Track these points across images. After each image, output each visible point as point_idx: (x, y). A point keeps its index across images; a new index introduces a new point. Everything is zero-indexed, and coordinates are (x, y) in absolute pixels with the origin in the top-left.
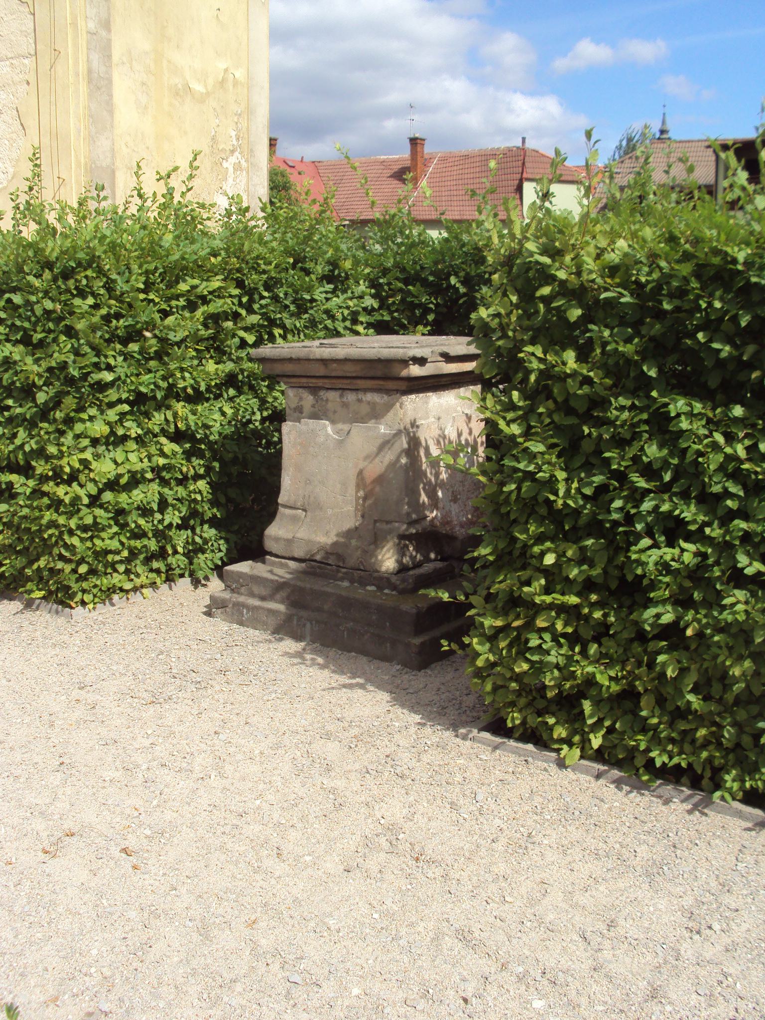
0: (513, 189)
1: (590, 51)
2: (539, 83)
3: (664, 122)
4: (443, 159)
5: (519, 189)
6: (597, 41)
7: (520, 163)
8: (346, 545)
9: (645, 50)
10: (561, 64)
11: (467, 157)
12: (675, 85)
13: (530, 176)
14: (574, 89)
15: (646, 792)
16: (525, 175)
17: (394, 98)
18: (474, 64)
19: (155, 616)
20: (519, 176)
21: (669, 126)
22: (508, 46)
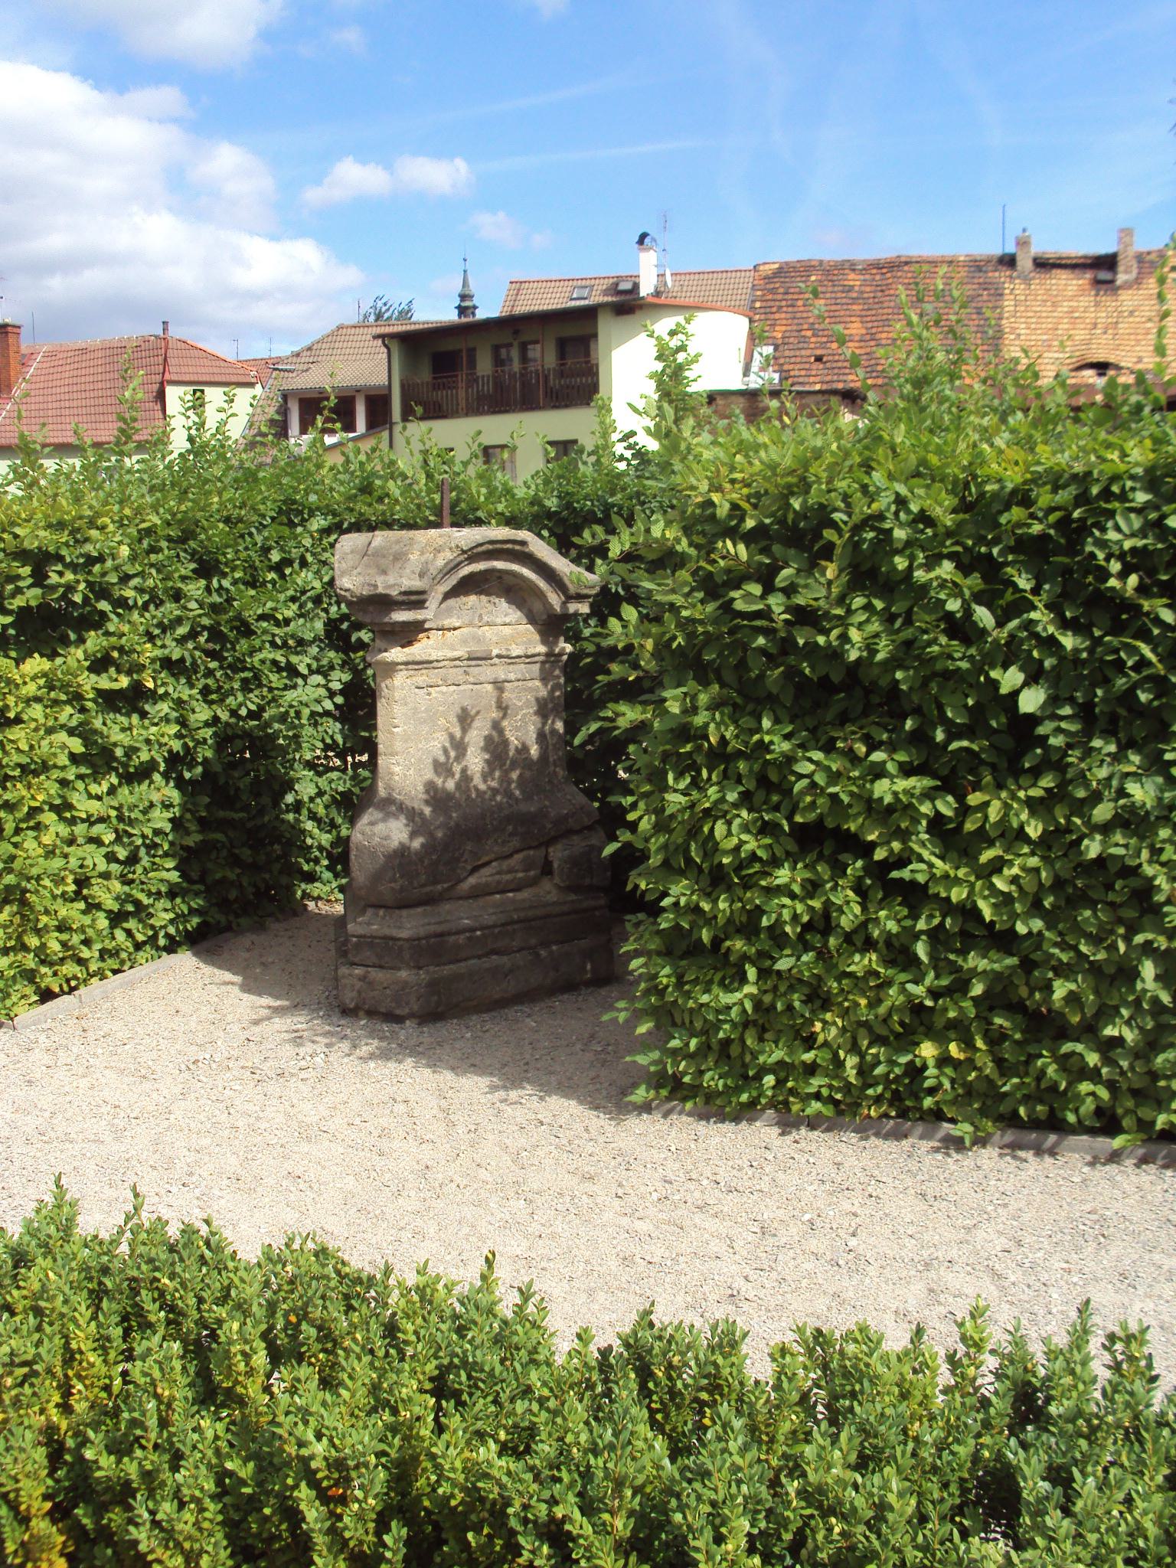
0: (151, 396)
1: (356, 177)
2: (287, 220)
3: (465, 284)
4: (50, 355)
5: (161, 396)
6: (363, 161)
7: (161, 359)
8: (1132, 989)
9: (438, 175)
10: (313, 195)
11: (84, 351)
12: (492, 225)
13: (175, 378)
14: (343, 229)
15: (1029, 1155)
16: (167, 377)
17: (55, 242)
18: (185, 194)
19: (222, 1202)
20: (159, 378)
21: (474, 288)
22: (227, 161)
